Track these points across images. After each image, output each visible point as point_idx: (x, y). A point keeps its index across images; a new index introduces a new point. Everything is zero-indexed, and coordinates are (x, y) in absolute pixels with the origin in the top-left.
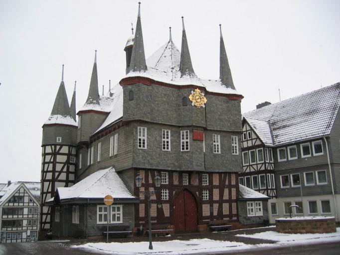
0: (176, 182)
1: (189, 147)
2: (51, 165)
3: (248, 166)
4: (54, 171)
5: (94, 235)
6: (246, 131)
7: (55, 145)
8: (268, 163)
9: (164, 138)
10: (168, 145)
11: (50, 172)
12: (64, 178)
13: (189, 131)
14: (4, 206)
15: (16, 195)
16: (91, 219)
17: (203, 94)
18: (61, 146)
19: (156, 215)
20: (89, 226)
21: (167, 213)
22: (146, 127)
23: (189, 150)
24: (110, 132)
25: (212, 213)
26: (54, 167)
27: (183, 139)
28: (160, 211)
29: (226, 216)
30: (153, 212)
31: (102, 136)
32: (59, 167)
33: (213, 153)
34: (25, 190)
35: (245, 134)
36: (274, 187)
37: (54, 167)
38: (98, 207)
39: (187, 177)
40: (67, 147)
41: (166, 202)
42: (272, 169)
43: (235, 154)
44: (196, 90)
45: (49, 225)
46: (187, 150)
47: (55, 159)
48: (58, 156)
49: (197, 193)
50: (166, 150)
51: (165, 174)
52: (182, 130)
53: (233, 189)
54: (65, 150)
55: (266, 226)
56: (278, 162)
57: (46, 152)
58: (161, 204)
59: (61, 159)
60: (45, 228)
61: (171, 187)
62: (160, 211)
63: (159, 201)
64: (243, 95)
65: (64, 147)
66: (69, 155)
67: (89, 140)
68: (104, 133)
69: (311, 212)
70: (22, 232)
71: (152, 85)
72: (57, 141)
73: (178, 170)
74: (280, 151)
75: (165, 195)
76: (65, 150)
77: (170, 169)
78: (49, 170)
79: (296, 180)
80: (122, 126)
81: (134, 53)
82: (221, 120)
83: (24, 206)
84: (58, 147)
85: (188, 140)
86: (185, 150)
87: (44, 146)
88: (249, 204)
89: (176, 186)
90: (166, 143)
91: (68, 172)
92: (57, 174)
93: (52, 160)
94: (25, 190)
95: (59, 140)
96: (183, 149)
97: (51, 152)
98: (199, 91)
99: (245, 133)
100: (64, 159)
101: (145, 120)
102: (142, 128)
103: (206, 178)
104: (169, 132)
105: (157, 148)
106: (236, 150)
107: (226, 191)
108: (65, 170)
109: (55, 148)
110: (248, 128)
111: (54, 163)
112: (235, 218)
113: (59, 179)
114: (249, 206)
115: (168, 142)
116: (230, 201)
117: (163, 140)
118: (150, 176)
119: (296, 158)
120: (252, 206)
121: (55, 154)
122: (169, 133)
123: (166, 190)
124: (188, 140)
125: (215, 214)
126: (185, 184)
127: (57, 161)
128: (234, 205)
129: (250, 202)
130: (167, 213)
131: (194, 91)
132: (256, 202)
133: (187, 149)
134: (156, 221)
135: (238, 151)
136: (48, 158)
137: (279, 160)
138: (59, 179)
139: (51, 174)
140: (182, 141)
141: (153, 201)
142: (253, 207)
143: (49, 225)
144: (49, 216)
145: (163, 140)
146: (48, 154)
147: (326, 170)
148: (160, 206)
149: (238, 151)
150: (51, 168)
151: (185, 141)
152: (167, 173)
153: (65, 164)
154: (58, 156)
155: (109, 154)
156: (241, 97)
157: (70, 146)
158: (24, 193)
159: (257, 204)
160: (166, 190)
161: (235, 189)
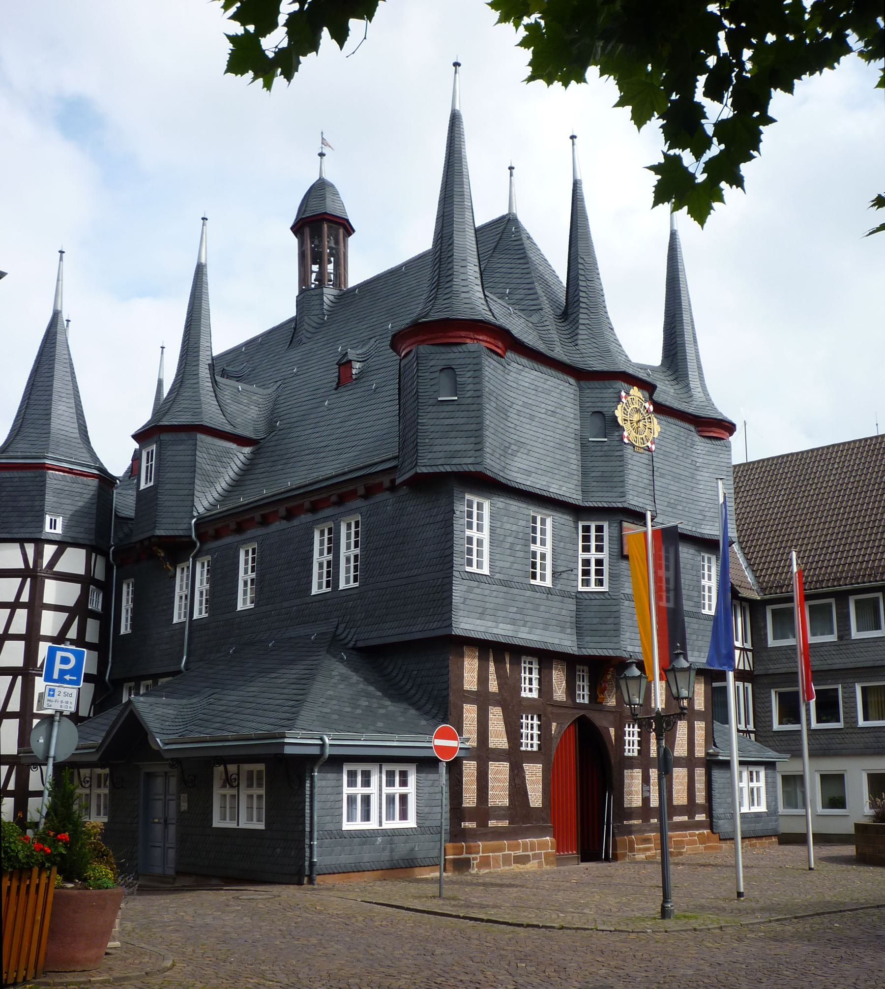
0: (559, 693)
2: (22, 615)
7: (39, 543)
8: (741, 649)
18: (62, 545)
19: (506, 802)
23: (605, 588)
25: (646, 800)
27: (586, 549)
29: (680, 810)
32: (50, 623)
37: (34, 623)
40: (82, 553)
42: (747, 668)
47: (37, 591)
49: (612, 731)
55: (305, 856)
56: (766, 647)
61: (544, 708)
66: (85, 581)
69: (823, 807)
71: (509, 354)
72: (47, 528)
74: (774, 612)
79: (828, 707)
81: (320, 226)
84: (49, 550)
85: (604, 555)
93: (25, 598)
95: (53, 525)
96: (586, 583)
97: (22, 566)
104: (549, 521)
109: (39, 554)
111: (35, 607)
112: (701, 817)
114: (352, 783)
116: (690, 762)
119: (833, 638)
120: (366, 783)
121: (32, 575)
122: (606, 534)
124: (582, 556)
125: (654, 803)
126: (582, 701)
127: (22, 644)
128: (700, 773)
132: (386, 767)
134: (505, 823)
137: (771, 642)
142: (373, 790)
147: (840, 687)
151: (593, 555)
157: (93, 549)
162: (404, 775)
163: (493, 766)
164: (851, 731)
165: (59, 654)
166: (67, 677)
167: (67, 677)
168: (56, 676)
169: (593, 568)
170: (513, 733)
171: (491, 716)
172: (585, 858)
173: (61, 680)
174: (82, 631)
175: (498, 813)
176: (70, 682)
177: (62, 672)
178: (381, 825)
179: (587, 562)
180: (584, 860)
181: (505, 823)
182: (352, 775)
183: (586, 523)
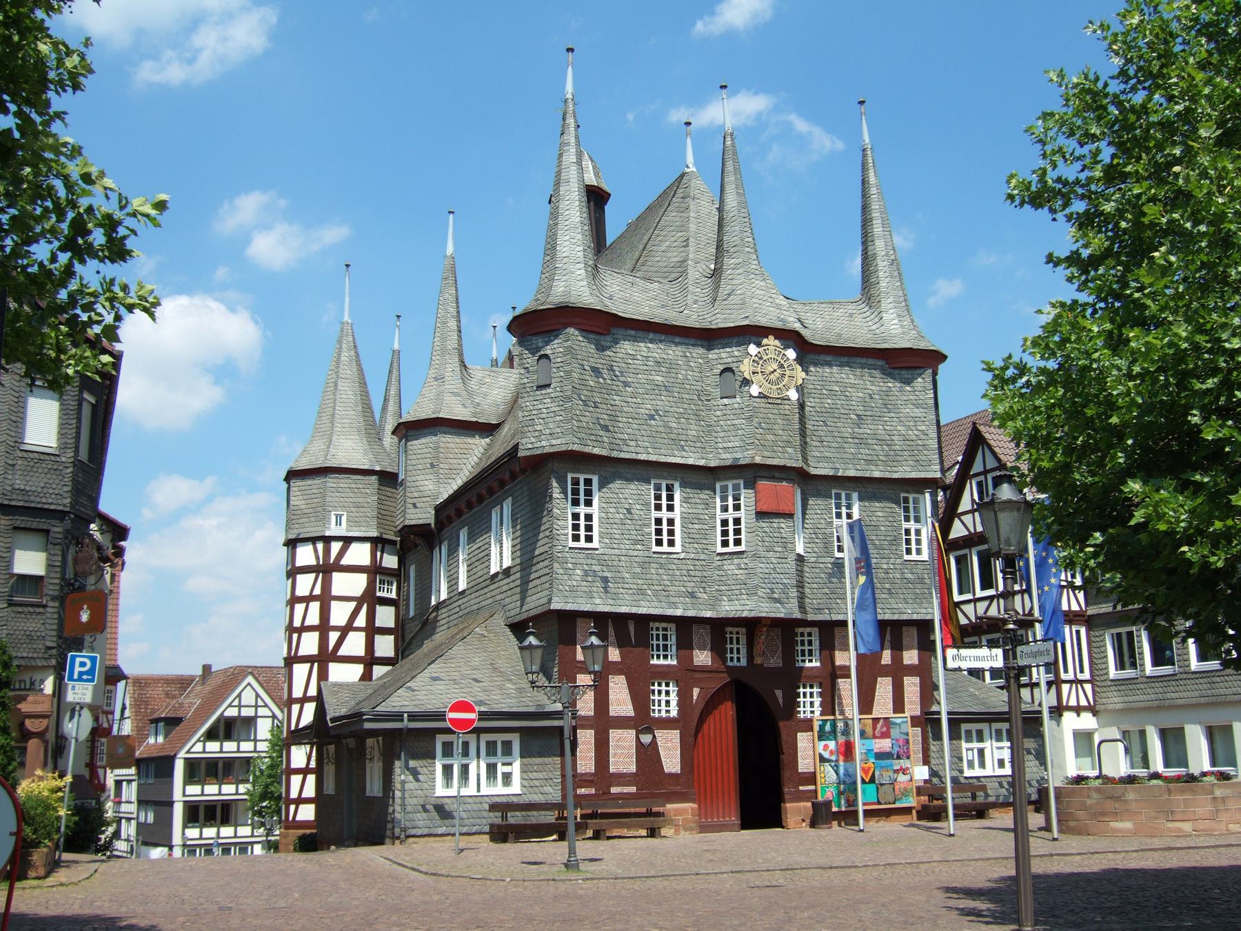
1: (719, 528)
2: (315, 607)
3: (991, 598)
4: (324, 627)
5: (425, 831)
6: (985, 472)
9: (907, 519)
10: (671, 533)
11: (311, 629)
12: (360, 651)
13: (742, 482)
14: (188, 752)
15: (226, 714)
16: (417, 780)
17: (791, 354)
18: (347, 541)
19: (633, 769)
20: (409, 801)
21: (671, 761)
22: (676, 480)
23: (742, 548)
24: (491, 492)
26: (325, 613)
28: (648, 755)
30: (623, 756)
31: (470, 505)
32: (340, 614)
33: (901, 557)
34: (257, 695)
35: (979, 484)
36: (1087, 675)
37: (325, 613)
38: (440, 739)
39: (743, 640)
40: (367, 547)
41: (667, 723)
42: (1075, 607)
43: (914, 557)
44: (765, 341)
45: (312, 807)
46: (671, 550)
47: (327, 585)
48: (335, 575)
49: (779, 693)
50: (665, 548)
51: (665, 629)
52: (720, 480)
53: (908, 681)
54: (360, 554)
57: (298, 564)
58: (649, 730)
59: (350, 585)
60: (299, 818)
62: (648, 755)
63: (643, 721)
64: (945, 352)
65: (355, 546)
67: (432, 521)
68: (462, 504)
70: (252, 843)
71: (614, 331)
73: (708, 614)
75: (666, 701)
76: (360, 554)
77: (679, 612)
78: (307, 624)
80: (523, 471)
82: (861, 441)
83: (255, 751)
86: (582, 543)
87: (292, 544)
88: (968, 733)
89: (703, 670)
90: (665, 527)
91: (372, 630)
92: (334, 637)
93: (317, 591)
94: (257, 695)
98: (777, 343)
99: (982, 478)
100: (354, 584)
101: (587, 450)
102: (582, 478)
103: (810, 643)
105: (636, 542)
106: (918, 542)
107: (884, 688)
108: (361, 621)
109: (327, 551)
110: (991, 463)
111: (326, 599)
113: (341, 652)
115: (671, 522)
117: (905, 525)
118: (888, 637)
123: (667, 685)
126: (735, 663)
127: (335, 592)
129: (974, 727)
130: (671, 761)
131: (759, 345)
132: (995, 726)
133: (737, 542)
134: (633, 789)
135: (925, 546)
136: (305, 583)
138: (341, 652)
139: (316, 635)
140: (720, 516)
141: (622, 723)
143: (312, 807)
144: (311, 779)
145: (905, 525)
146: (306, 570)
148: (646, 739)
149: (925, 546)
150: (313, 618)
151: (731, 515)
152: (673, 626)
153: (360, 601)
154: (335, 575)
155: (488, 567)
156: (943, 358)
157: (378, 543)
158: (256, 706)
159: (999, 732)
160: (667, 685)
161: (917, 680)
162: (507, 746)
163: (614, 734)
164: (1185, 676)
165: (78, 660)
166: (85, 677)
167: (85, 677)
168: (76, 677)
169: (731, 527)
170: (641, 699)
171: (611, 685)
172: (749, 821)
173: (80, 679)
174: (371, 616)
175: (621, 778)
176: (87, 680)
177: (81, 673)
178: (479, 790)
179: (725, 523)
180: (744, 826)
181: (633, 789)
182: (968, 733)
183: (725, 483)
